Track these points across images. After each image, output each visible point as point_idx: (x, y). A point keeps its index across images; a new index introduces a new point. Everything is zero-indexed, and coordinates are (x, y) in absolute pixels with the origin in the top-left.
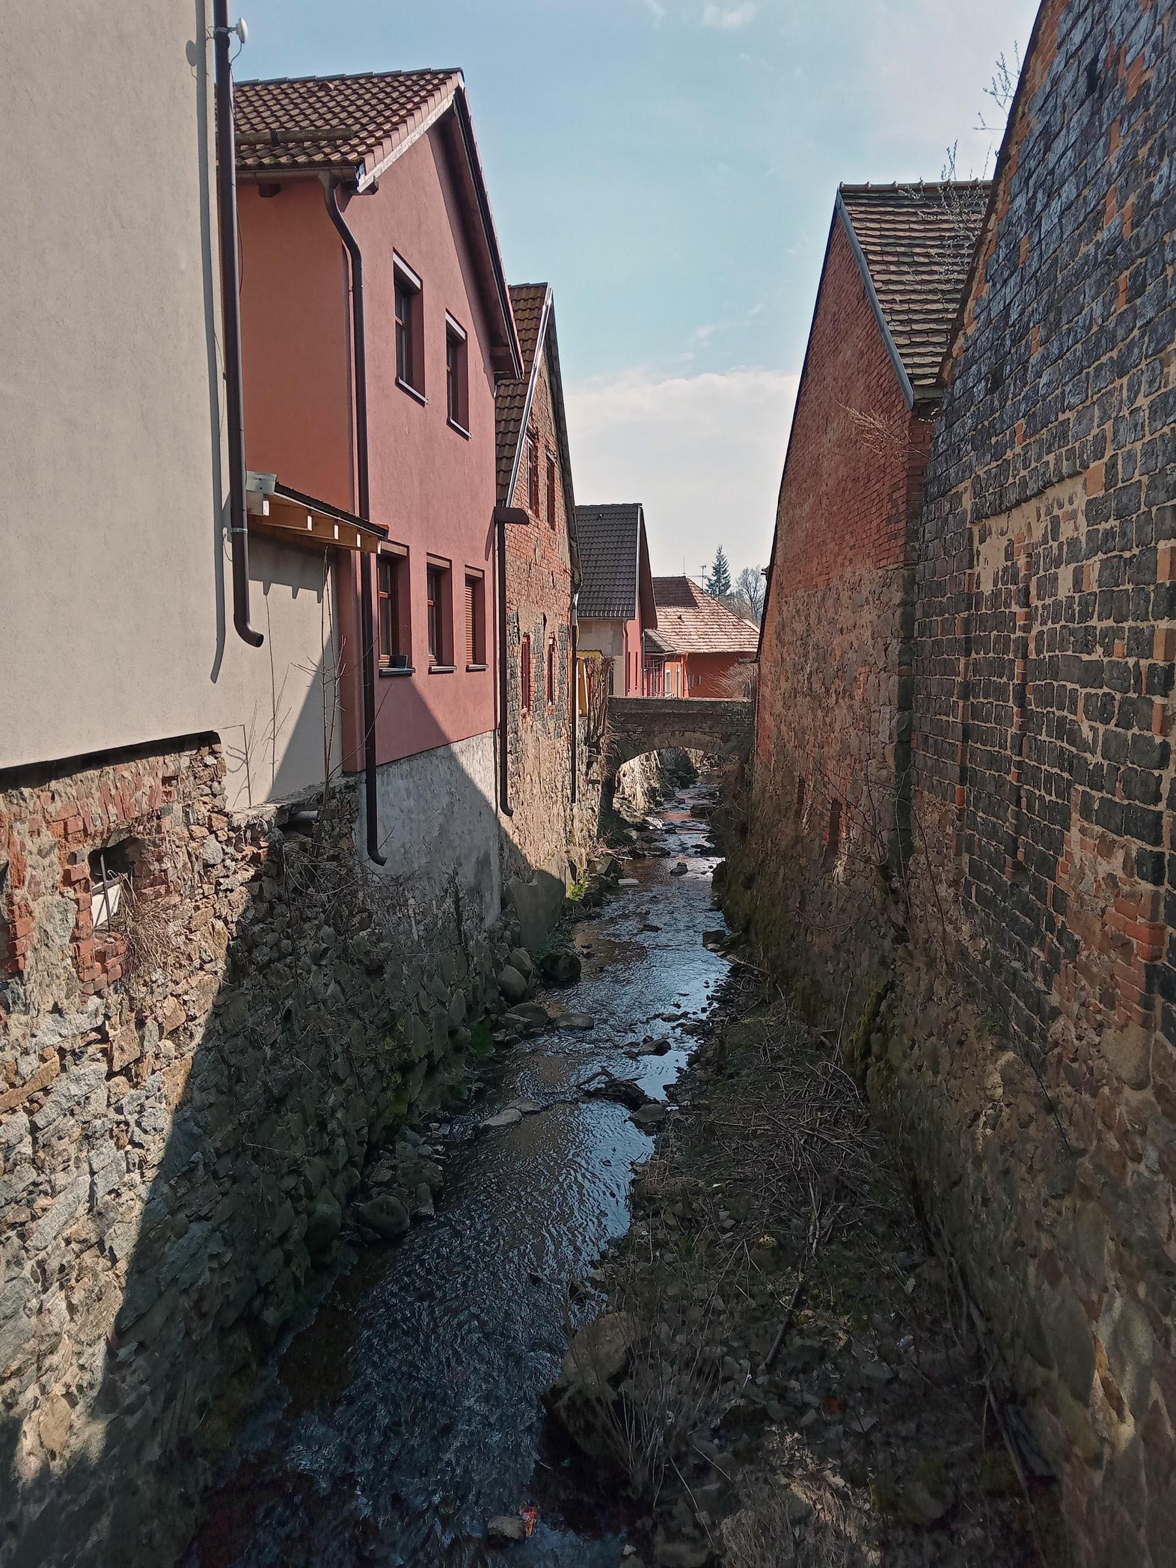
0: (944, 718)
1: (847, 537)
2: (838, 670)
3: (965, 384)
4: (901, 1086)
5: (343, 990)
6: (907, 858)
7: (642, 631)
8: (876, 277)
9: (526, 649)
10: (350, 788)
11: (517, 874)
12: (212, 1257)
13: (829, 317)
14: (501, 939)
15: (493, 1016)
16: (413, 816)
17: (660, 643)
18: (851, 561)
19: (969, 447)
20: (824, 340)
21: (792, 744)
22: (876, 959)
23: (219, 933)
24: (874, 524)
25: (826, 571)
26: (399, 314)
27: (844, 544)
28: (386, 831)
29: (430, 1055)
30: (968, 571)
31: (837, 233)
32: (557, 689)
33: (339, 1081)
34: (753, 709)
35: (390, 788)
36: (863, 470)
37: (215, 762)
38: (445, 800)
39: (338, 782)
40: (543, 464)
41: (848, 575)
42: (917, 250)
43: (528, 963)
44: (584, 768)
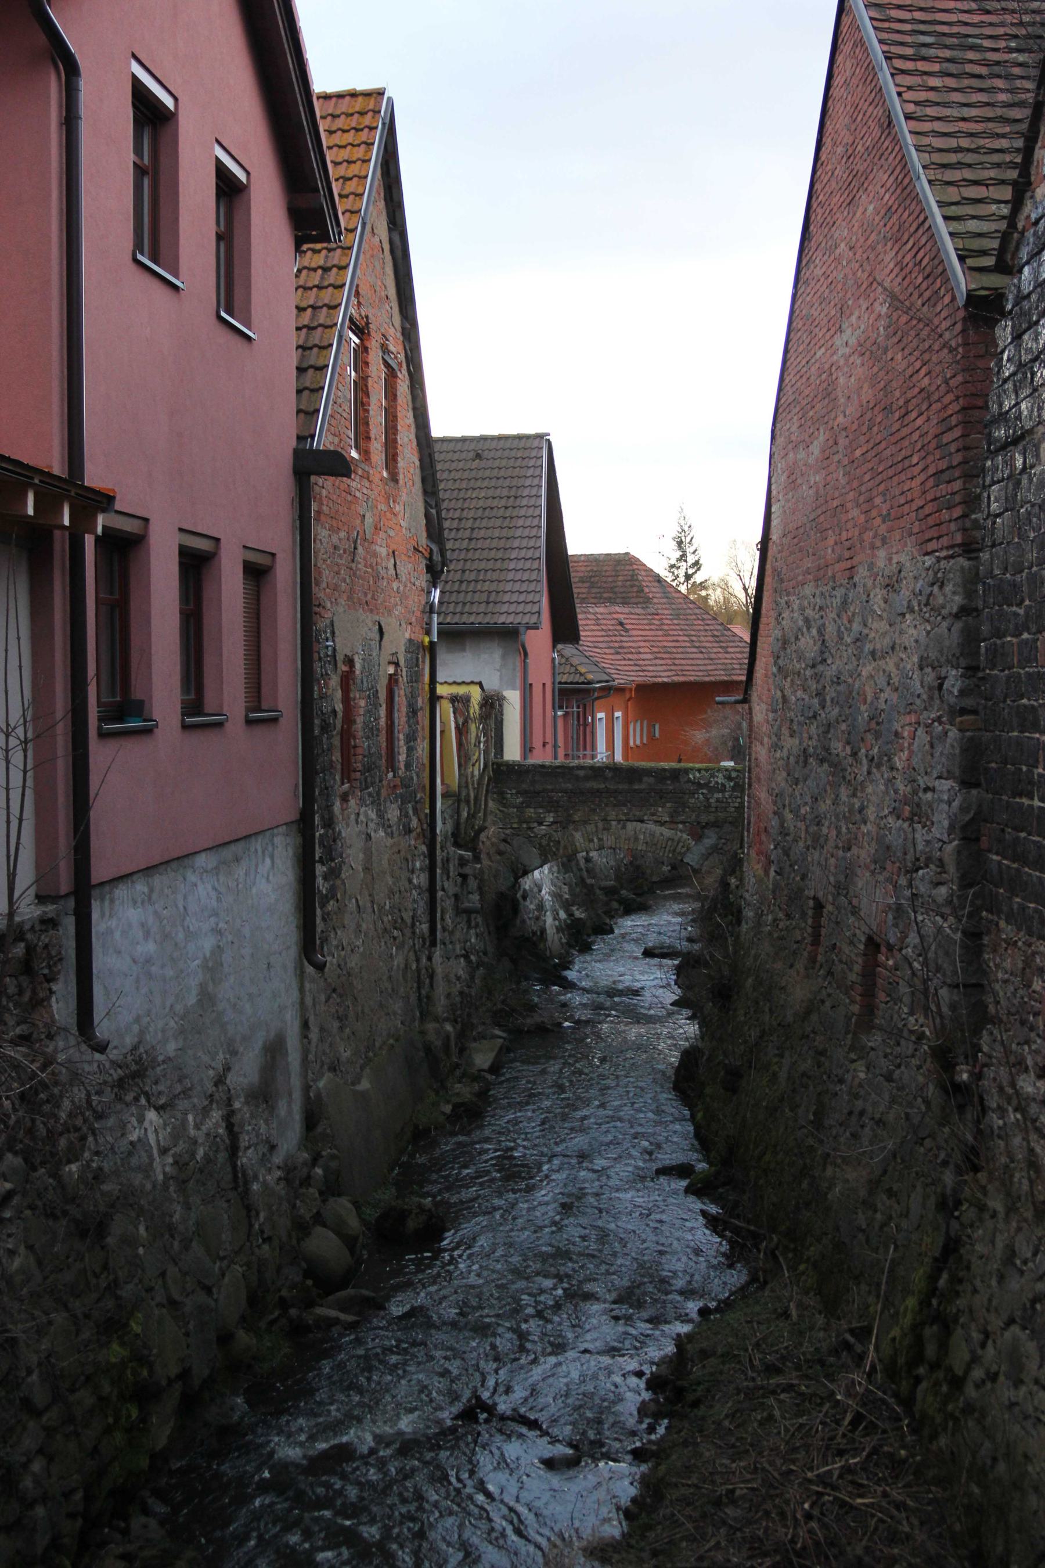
0: (1025, 801)
1: (878, 501)
2: (871, 719)
4: (969, 1409)
5: (40, 1263)
6: (977, 1031)
8: (906, 96)
9: (347, 680)
10: (49, 923)
11: (333, 1069)
13: (840, 150)
14: (307, 1181)
15: (293, 1312)
16: (154, 969)
20: (833, 184)
21: (801, 844)
22: (932, 1201)
25: (847, 555)
26: (138, 150)
27: (874, 513)
28: (107, 994)
29: (185, 1375)
31: (846, 20)
32: (403, 750)
33: (36, 1413)
34: (739, 783)
35: (113, 923)
36: (897, 394)
38: (208, 944)
39: (28, 911)
40: (377, 371)
41: (881, 563)
42: (971, 55)
43: (353, 1223)
44: (451, 887)
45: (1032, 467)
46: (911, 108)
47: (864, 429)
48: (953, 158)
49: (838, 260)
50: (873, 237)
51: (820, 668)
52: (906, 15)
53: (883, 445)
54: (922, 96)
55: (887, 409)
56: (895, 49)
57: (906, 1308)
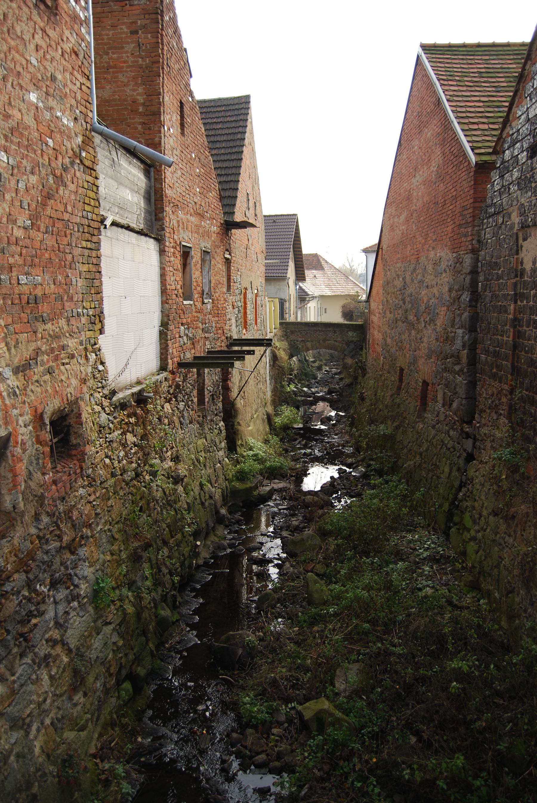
3: (513, 153)
7: (296, 285)
12: (114, 643)
17: (307, 290)
18: (433, 248)
19: (516, 188)
20: (412, 125)
23: (107, 466)
24: (450, 228)
25: (416, 253)
27: (429, 239)
30: (515, 257)
36: (440, 198)
37: (103, 368)
45: (507, 222)
46: (448, 97)
47: (425, 210)
48: (464, 115)
49: (414, 152)
50: (431, 143)
51: (403, 291)
52: (443, 65)
53: (433, 216)
54: (451, 93)
55: (436, 203)
56: (440, 77)
57: (212, 688)
